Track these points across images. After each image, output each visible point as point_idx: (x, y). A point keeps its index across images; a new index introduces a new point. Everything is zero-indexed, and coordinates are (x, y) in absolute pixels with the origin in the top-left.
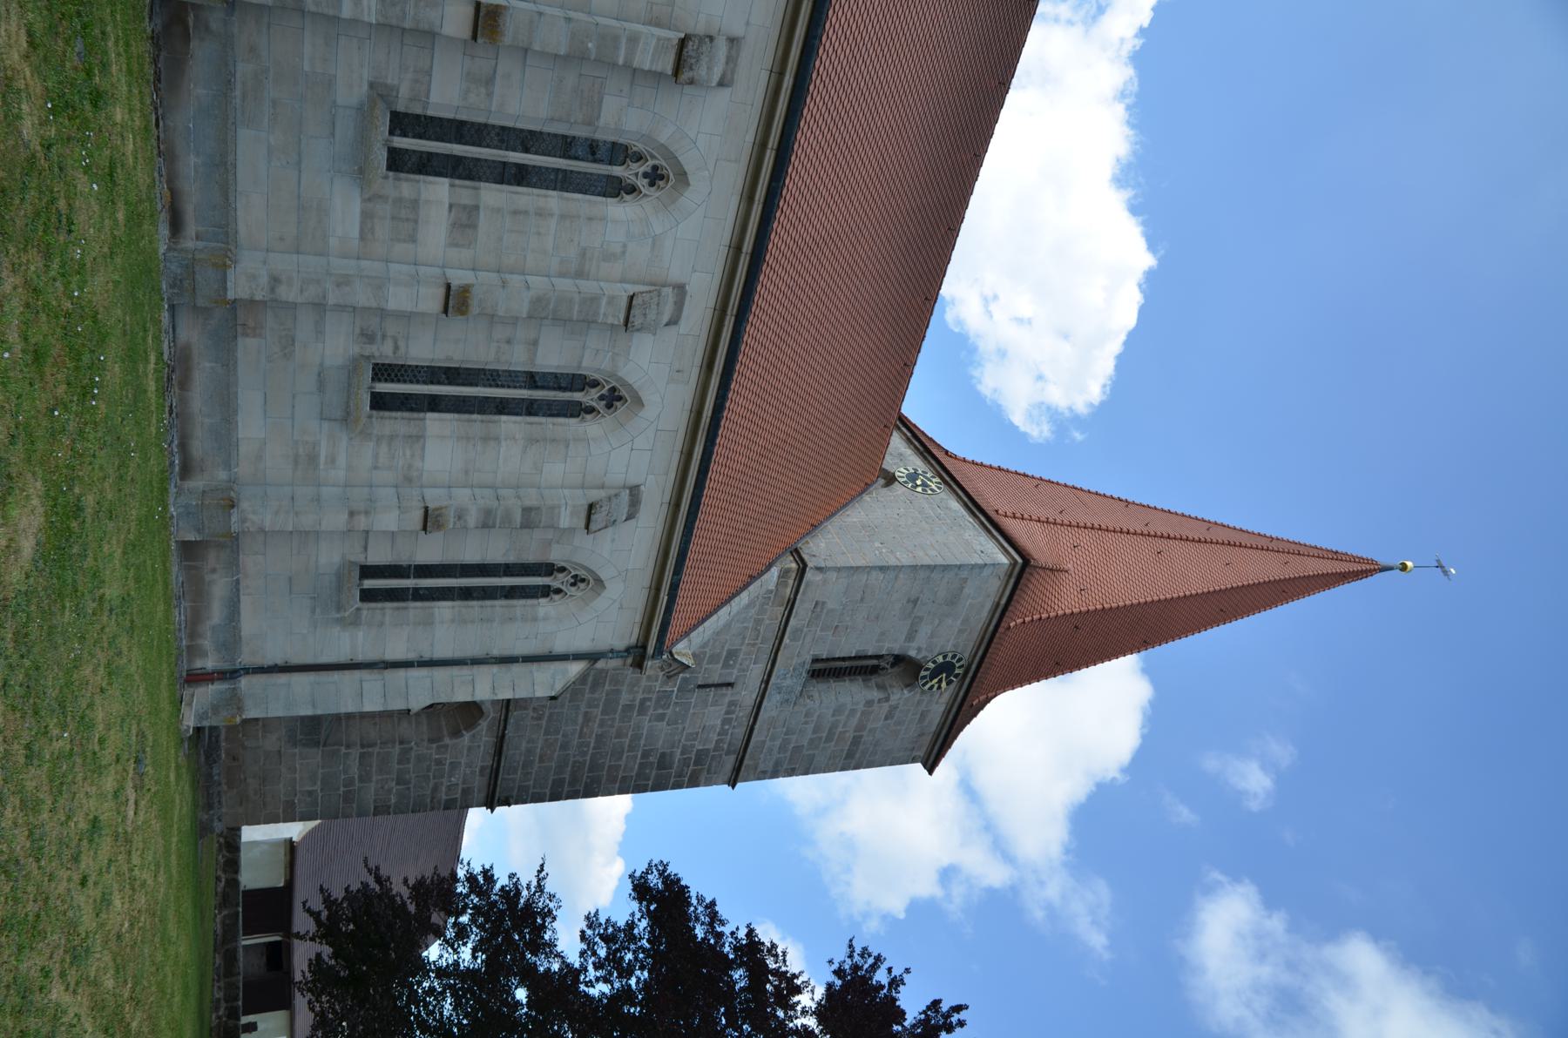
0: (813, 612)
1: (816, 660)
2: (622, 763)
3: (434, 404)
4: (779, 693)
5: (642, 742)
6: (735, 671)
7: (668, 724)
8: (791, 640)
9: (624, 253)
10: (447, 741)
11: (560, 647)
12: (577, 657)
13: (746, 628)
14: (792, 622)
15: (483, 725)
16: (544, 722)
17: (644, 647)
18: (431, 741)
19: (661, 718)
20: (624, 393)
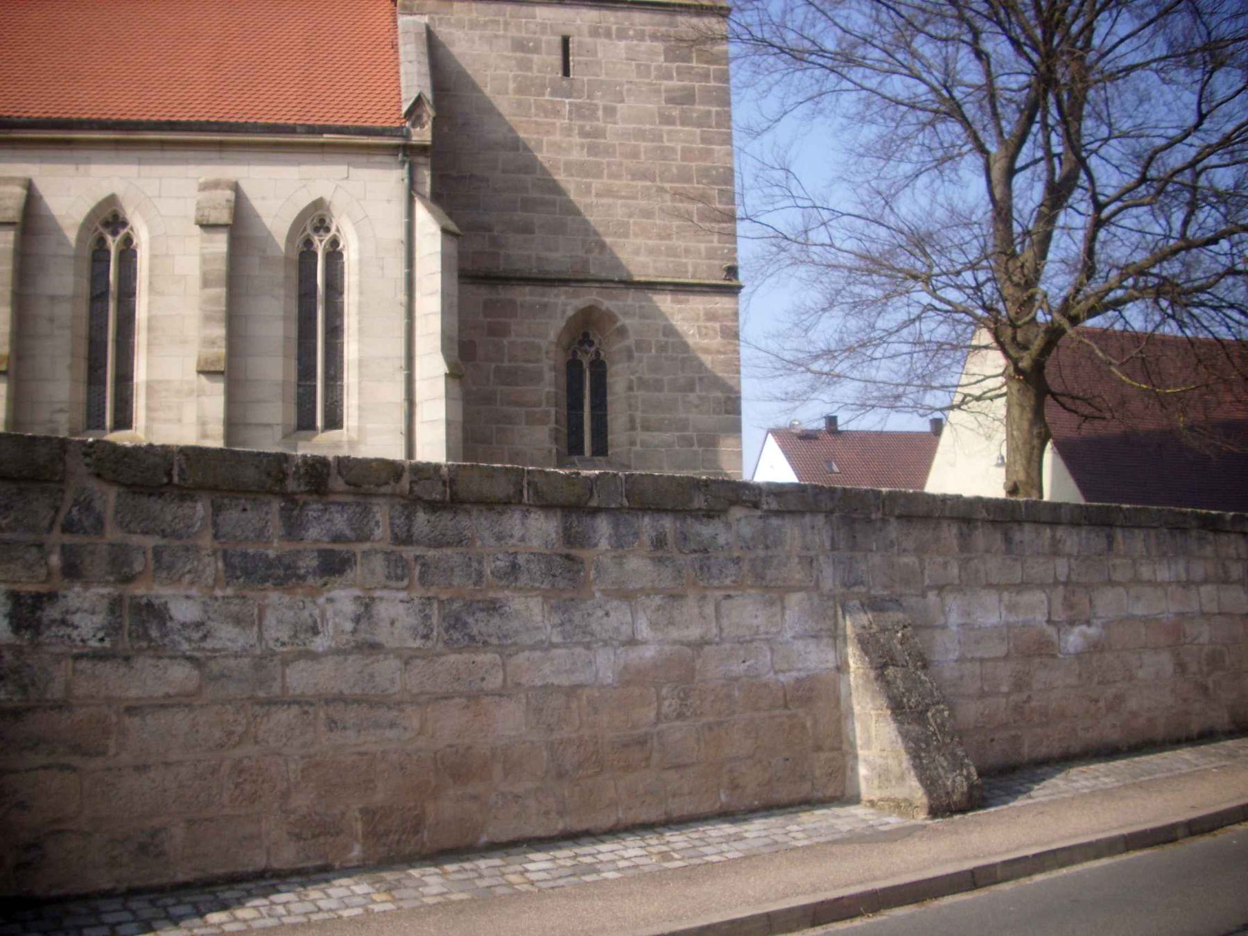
5: (648, 127)
7: (622, 101)
10: (631, 341)
13: (481, 37)
15: (607, 304)
17: (397, 147)
18: (630, 357)
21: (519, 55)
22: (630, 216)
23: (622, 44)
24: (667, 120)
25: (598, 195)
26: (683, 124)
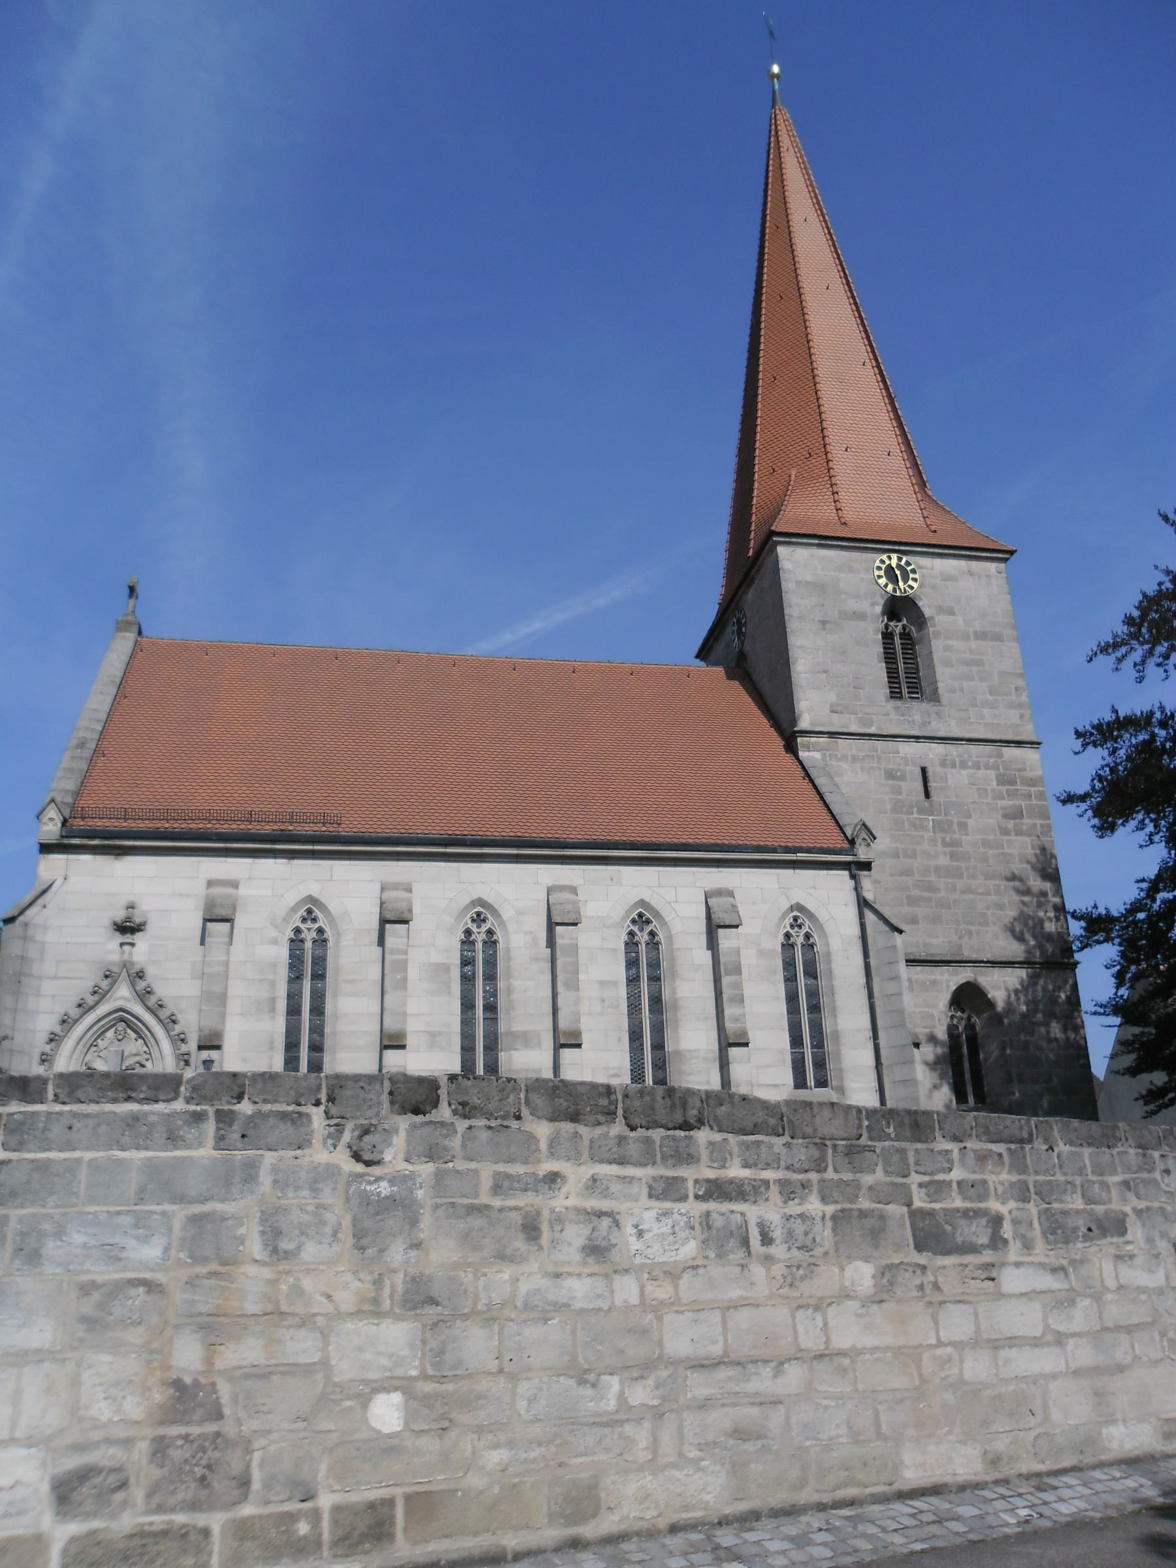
0: (842, 713)
1: (895, 694)
2: (1016, 852)
3: (658, 1046)
4: (930, 723)
5: (991, 837)
6: (908, 769)
7: (970, 817)
8: (872, 725)
9: (531, 933)
11: (856, 931)
12: (861, 916)
13: (861, 768)
14: (853, 728)
16: (974, 928)
19: (963, 826)
20: (634, 915)
21: (890, 782)
22: (988, 908)
23: (964, 772)
24: (1006, 832)
25: (962, 892)
26: (1016, 835)
